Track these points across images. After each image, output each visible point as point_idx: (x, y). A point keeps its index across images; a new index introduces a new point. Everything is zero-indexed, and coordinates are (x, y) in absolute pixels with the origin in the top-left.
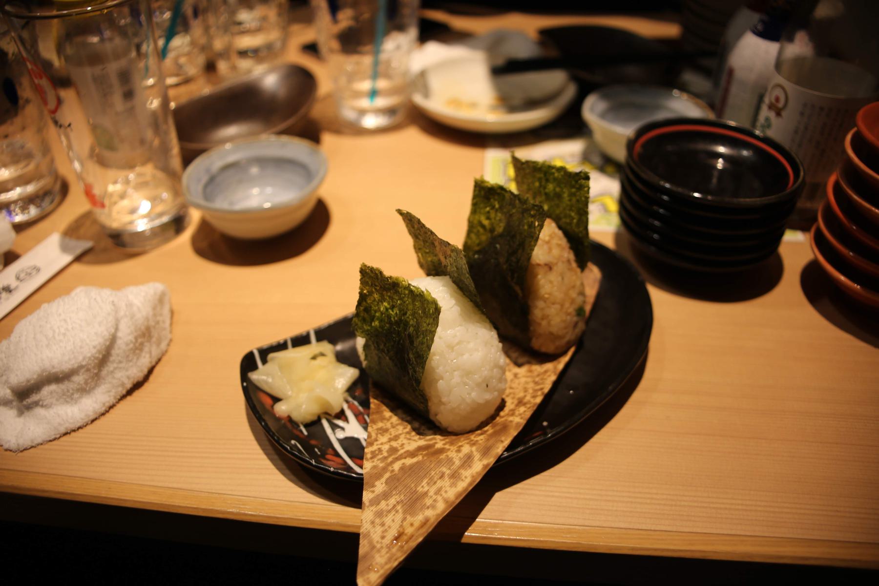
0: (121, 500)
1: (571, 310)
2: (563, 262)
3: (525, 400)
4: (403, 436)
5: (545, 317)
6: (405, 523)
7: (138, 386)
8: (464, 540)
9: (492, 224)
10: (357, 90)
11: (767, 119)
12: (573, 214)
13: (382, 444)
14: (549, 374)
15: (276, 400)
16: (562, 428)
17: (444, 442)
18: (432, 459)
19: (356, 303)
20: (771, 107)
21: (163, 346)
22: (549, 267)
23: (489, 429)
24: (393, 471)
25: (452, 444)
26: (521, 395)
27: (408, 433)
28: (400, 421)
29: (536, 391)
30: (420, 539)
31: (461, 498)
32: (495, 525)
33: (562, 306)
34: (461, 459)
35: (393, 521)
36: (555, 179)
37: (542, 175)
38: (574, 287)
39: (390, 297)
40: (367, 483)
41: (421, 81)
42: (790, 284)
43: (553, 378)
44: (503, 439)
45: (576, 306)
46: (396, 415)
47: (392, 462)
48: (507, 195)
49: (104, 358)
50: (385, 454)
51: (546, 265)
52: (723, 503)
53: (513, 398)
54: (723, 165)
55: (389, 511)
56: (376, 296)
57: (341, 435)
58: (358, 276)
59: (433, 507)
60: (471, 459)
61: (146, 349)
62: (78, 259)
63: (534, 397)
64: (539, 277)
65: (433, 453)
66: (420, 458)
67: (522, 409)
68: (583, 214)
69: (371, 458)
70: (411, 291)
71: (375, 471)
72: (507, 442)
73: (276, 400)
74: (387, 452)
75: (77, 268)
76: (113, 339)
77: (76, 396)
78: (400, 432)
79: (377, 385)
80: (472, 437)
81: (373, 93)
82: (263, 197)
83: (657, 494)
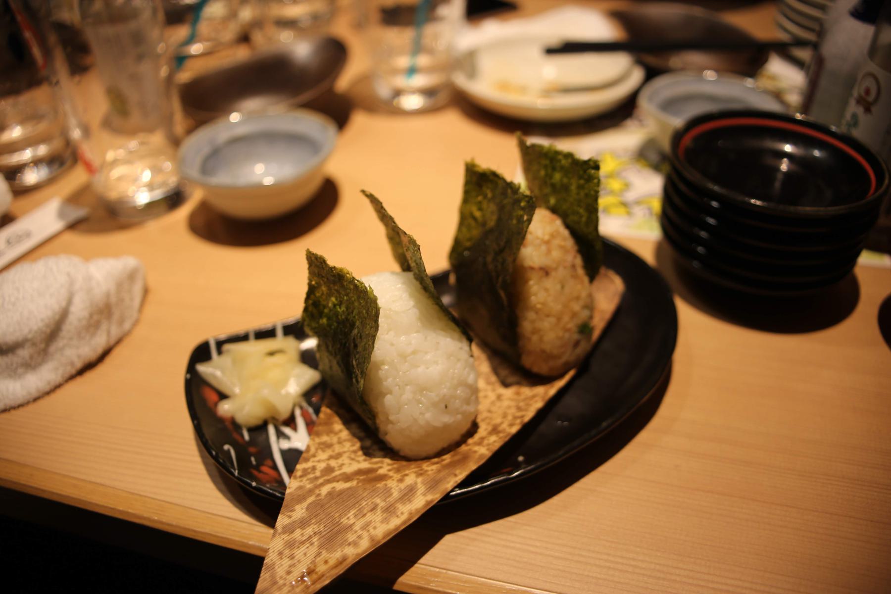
0: (39, 489)
1: (571, 325)
2: (565, 268)
3: (500, 428)
4: (345, 456)
5: (536, 331)
6: (318, 559)
7: (89, 366)
8: (397, 587)
9: (483, 216)
10: (392, 65)
11: (855, 116)
12: (581, 211)
13: (319, 461)
14: (536, 399)
15: (223, 396)
16: (532, 467)
17: (390, 467)
18: (368, 486)
19: (304, 296)
20: (860, 101)
21: (127, 325)
22: (546, 272)
23: (447, 458)
24: (319, 495)
25: (398, 470)
26: (498, 420)
27: (355, 452)
28: (350, 437)
29: (515, 418)
30: (327, 582)
31: (388, 538)
32: (437, 575)
33: (559, 319)
34: (401, 491)
35: (305, 554)
36: (562, 168)
37: (547, 162)
38: (578, 298)
39: (337, 291)
40: (287, 506)
41: (467, 62)
42: (864, 318)
43: (539, 404)
44: (457, 472)
45: (579, 321)
46: (348, 428)
47: (322, 485)
48: (500, 182)
49: (53, 333)
50: (318, 474)
51: (541, 269)
52: (726, 584)
53: (489, 424)
54: (788, 167)
55: (303, 543)
56: (324, 288)
57: (285, 445)
58: (305, 265)
59: (355, 544)
60: (413, 493)
61: (104, 326)
62: (73, 226)
63: (511, 425)
64: (531, 283)
65: (370, 478)
66: (354, 483)
67: (493, 438)
68: (592, 211)
69: (301, 477)
70: (356, 286)
71: (300, 492)
72: (462, 475)
73: (223, 396)
74: (322, 471)
75: (71, 238)
76: (64, 315)
77: (20, 371)
78: (345, 449)
79: (335, 393)
80: (425, 466)
81: (412, 71)
82: (267, 174)
83: (642, 561)
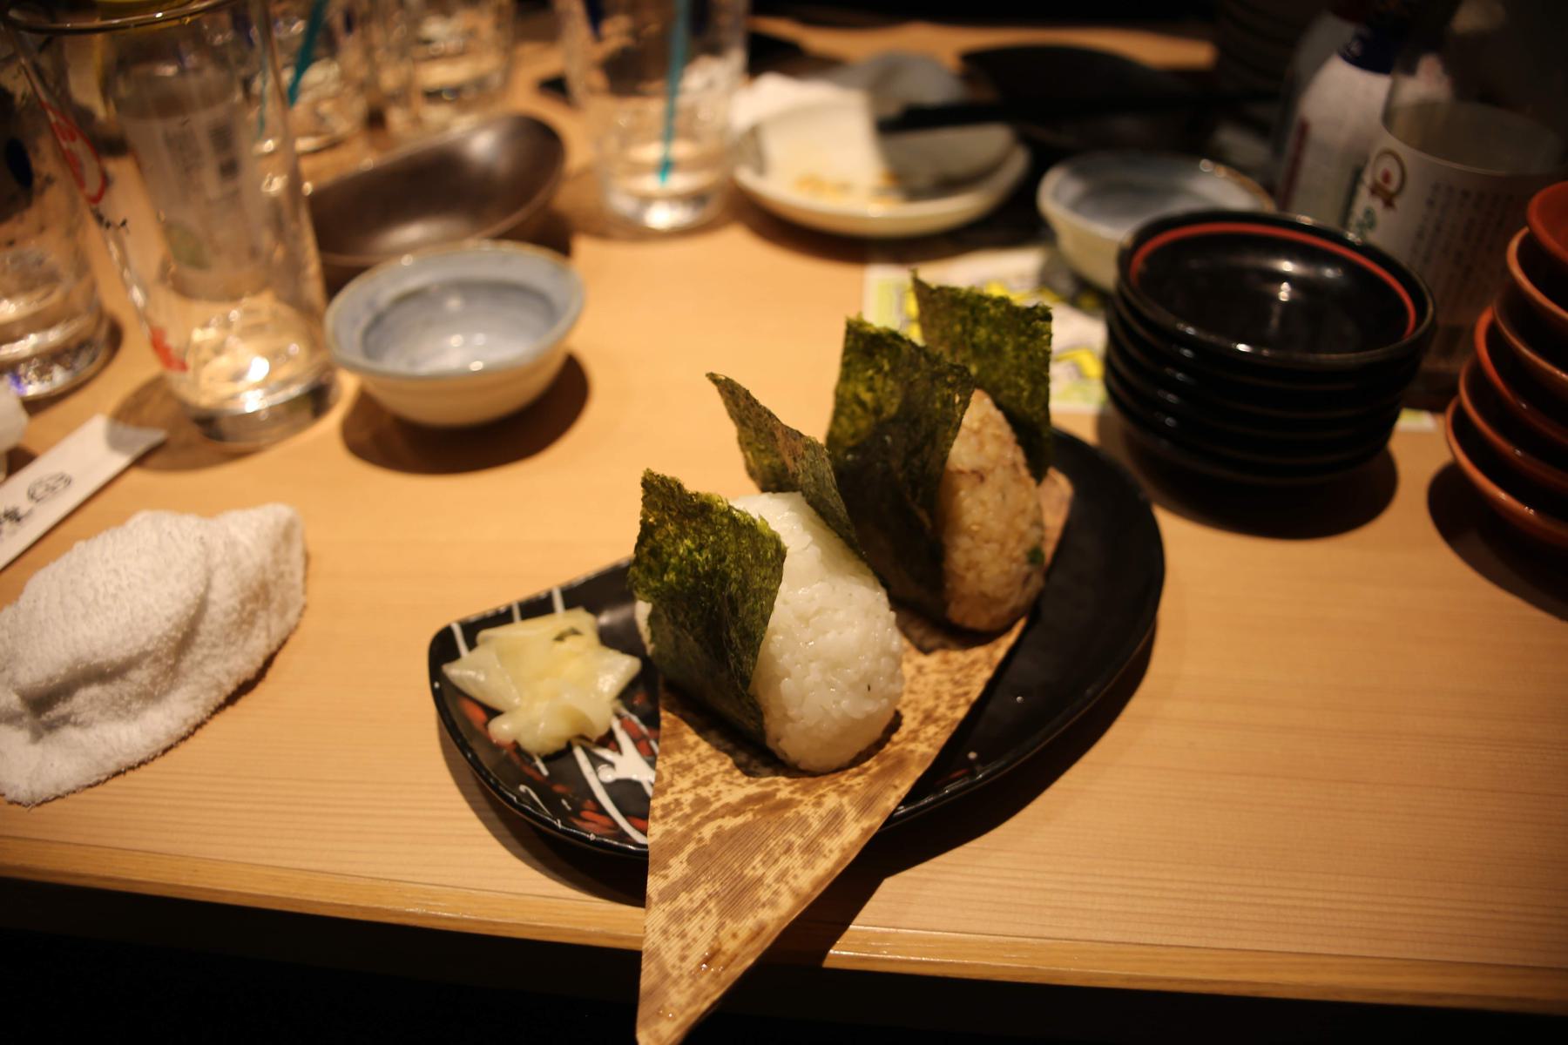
0: (217, 891)
1: (1019, 553)
2: (1004, 467)
3: (937, 714)
4: (718, 778)
5: (972, 565)
6: (722, 933)
7: (246, 688)
8: (827, 964)
9: (877, 400)
10: (637, 160)
11: (1369, 213)
12: (1022, 382)
13: (681, 792)
14: (978, 666)
15: (493, 713)
16: (1003, 763)
17: (791, 788)
18: (771, 818)
19: (635, 541)
20: (1375, 190)
21: (291, 617)
22: (980, 476)
23: (872, 765)
24: (701, 840)
25: (806, 791)
26: (930, 704)
27: (727, 772)
28: (713, 752)
29: (955, 697)
30: (750, 962)
31: (823, 888)
32: (883, 937)
33: (1003, 545)
34: (822, 818)
35: (701, 928)
36: (990, 320)
37: (967, 313)
38: (1023, 512)
39: (695, 530)
40: (656, 862)
41: (750, 145)
42: (1409, 506)
43: (987, 674)
44: (897, 782)
45: (1027, 546)
46: (706, 740)
47: (700, 825)
48: (905, 348)
49: (185, 639)
50: (687, 810)
51: (974, 472)
52: (1289, 898)
53: (915, 710)
54: (1290, 293)
55: (694, 912)
56: (671, 528)
57: (608, 775)
58: (639, 492)
59: (772, 903)
60: (840, 819)
61: (261, 622)
62: (139, 462)
63: (953, 708)
64: (962, 493)
65: (773, 807)
66: (749, 816)
67: (931, 730)
68: (1041, 381)
69: (663, 817)
70: (734, 520)
71: (669, 840)
72: (904, 787)
73: (493, 713)
74: (691, 805)
75: (138, 477)
76: (202, 605)
77: (135, 706)
78: (714, 770)
79: (672, 686)
80: (843, 779)
81: (666, 167)
82: (469, 352)
83: (1172, 881)
